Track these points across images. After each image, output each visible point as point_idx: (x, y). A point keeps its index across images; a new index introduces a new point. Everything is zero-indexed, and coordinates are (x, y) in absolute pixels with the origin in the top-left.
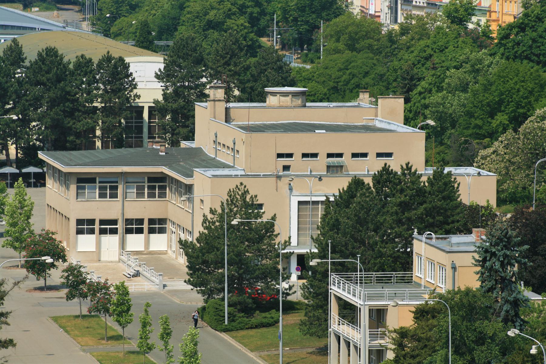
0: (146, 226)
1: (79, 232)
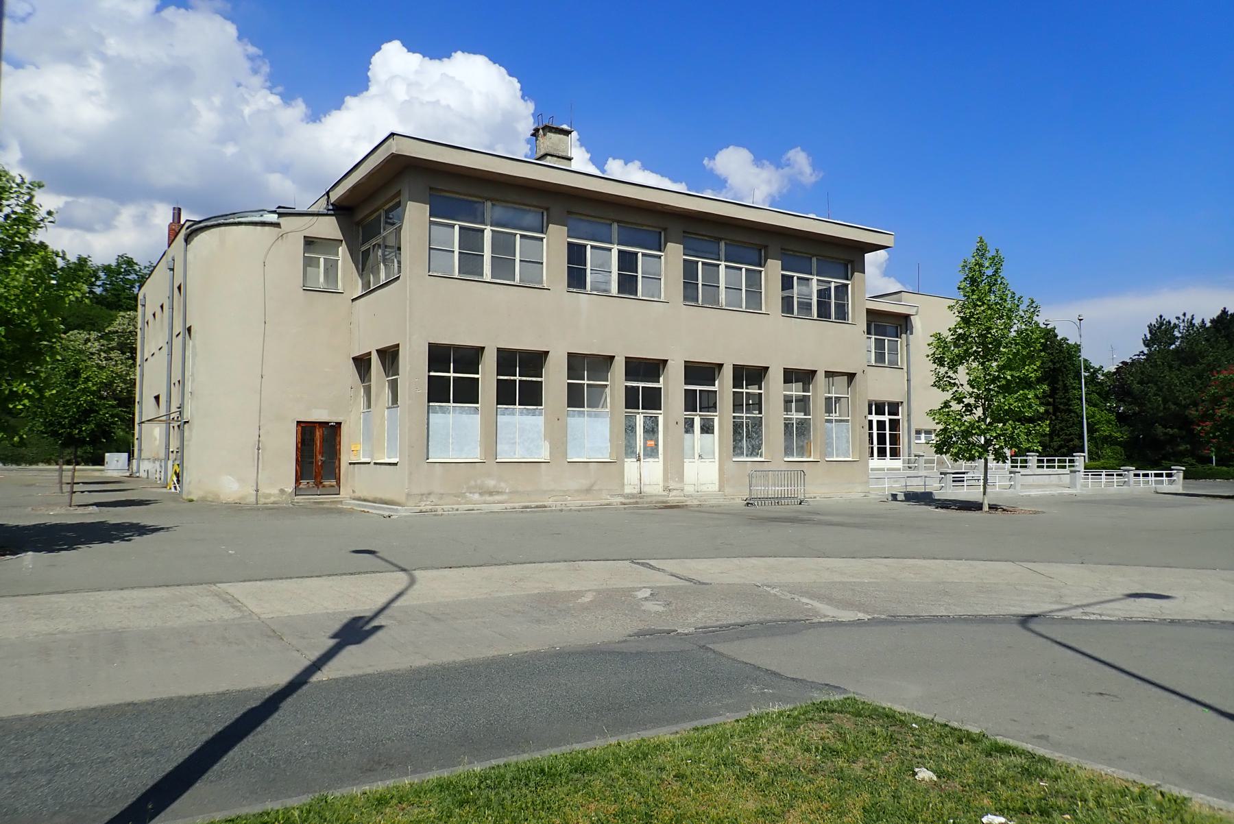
0: (487, 376)
1: (437, 391)
